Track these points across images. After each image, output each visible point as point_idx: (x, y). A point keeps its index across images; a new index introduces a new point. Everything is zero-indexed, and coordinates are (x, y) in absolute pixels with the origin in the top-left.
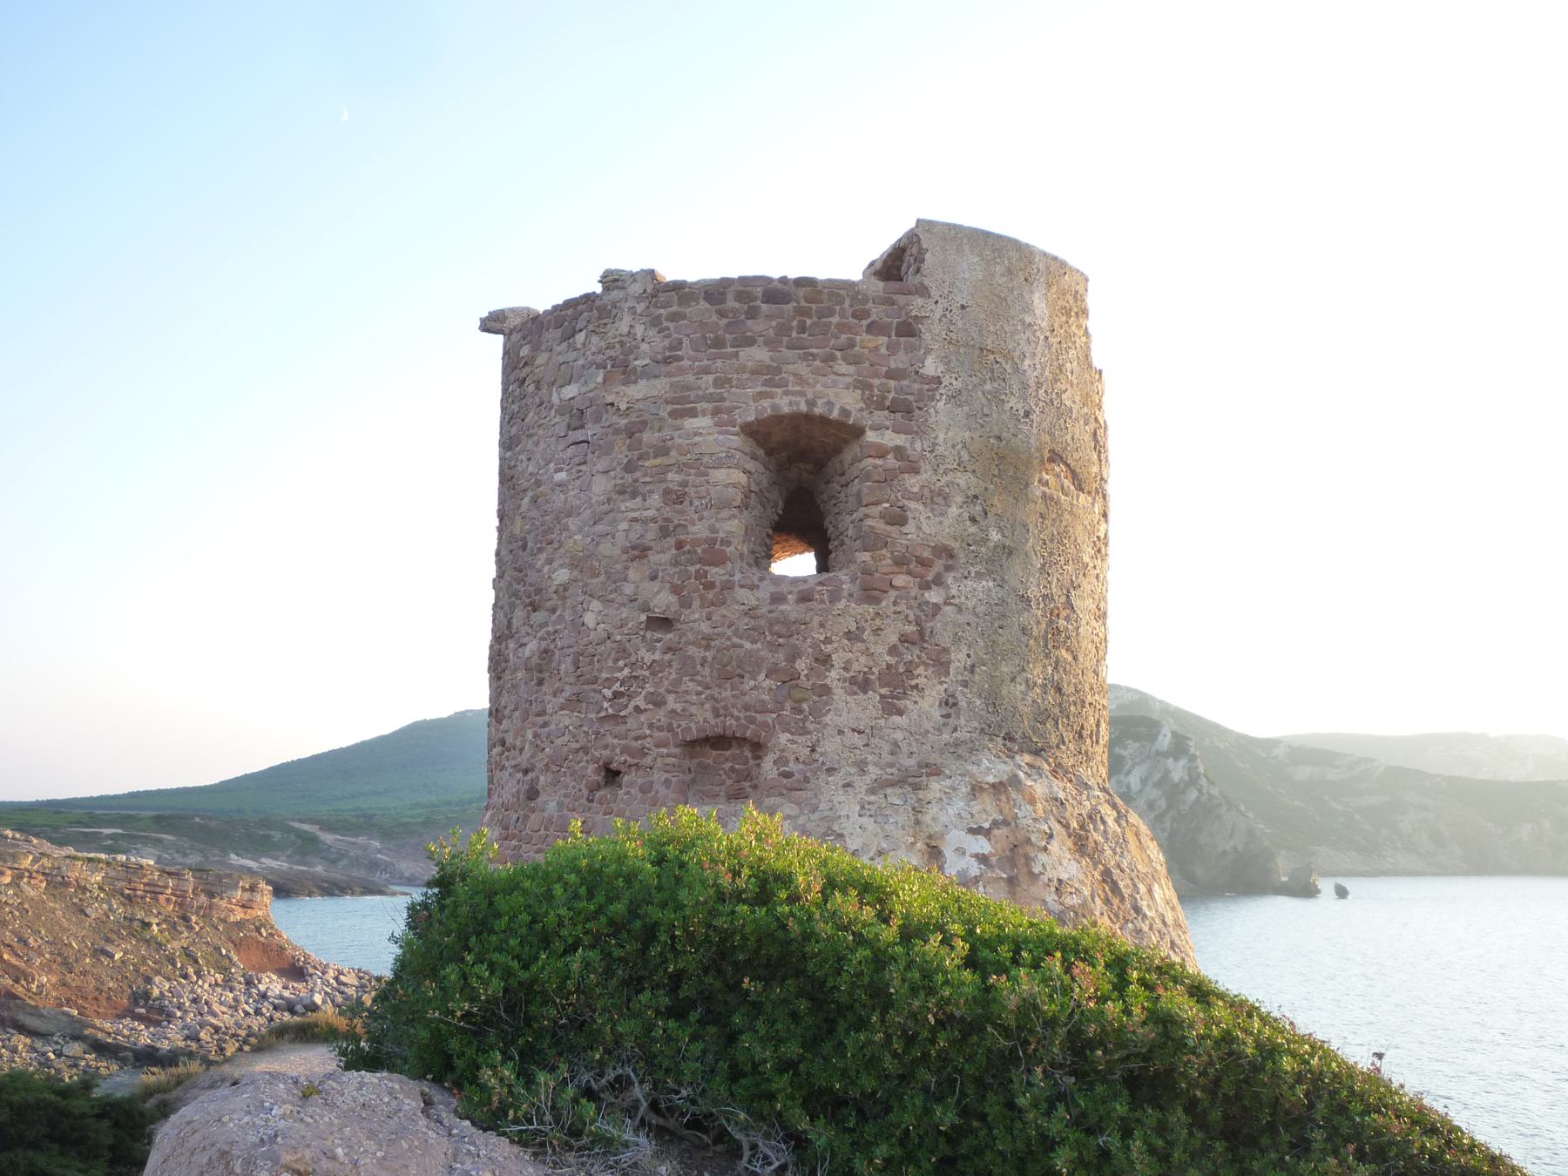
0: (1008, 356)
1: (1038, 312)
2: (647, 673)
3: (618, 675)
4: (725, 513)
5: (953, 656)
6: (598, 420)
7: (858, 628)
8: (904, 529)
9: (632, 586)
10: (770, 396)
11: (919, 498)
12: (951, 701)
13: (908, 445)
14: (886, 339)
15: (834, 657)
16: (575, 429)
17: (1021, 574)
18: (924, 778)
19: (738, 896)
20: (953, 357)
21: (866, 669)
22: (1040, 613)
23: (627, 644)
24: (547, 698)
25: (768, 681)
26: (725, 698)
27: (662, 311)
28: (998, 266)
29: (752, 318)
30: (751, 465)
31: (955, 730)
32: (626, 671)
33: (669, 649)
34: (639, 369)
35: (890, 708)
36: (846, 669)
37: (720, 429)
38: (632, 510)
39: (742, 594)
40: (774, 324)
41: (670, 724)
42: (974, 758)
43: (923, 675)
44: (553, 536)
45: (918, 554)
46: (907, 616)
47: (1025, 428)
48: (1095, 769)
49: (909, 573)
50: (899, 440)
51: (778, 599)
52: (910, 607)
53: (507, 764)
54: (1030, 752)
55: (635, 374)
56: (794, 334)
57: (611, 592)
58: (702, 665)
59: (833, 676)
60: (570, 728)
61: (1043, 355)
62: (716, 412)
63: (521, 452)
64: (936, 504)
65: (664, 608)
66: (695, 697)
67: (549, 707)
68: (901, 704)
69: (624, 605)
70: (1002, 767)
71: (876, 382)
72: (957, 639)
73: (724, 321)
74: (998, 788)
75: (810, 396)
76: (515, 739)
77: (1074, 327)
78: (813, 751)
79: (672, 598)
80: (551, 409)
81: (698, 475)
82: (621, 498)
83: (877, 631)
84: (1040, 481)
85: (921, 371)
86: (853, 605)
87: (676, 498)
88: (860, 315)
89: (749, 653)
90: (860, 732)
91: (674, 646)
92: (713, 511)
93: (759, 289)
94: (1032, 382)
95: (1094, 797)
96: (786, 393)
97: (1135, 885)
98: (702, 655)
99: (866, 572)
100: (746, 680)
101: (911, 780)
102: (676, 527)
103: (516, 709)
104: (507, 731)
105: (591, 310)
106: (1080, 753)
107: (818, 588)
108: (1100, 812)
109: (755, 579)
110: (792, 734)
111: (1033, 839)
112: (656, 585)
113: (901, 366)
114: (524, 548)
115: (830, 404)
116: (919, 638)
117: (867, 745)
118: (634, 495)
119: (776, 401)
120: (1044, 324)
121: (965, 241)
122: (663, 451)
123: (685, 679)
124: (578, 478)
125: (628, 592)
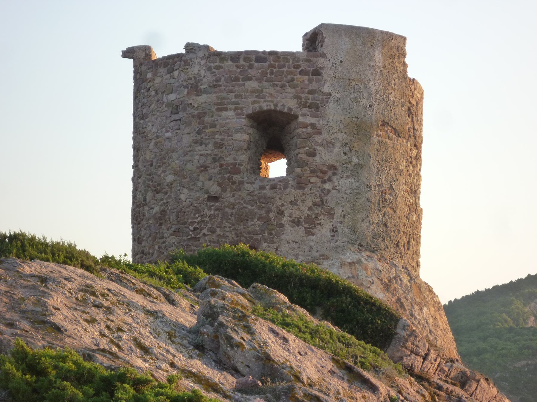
0: (362, 81)
1: (377, 60)
2: (208, 219)
3: (196, 220)
4: (240, 153)
5: (336, 211)
6: (185, 110)
7: (295, 200)
8: (315, 158)
10: (258, 102)
11: (321, 145)
12: (335, 229)
13: (317, 123)
14: (307, 77)
15: (285, 212)
16: (175, 114)
17: (367, 176)
18: (322, 260)
19: (238, 255)
20: (336, 84)
21: (299, 217)
22: (376, 192)
23: (199, 207)
24: (164, 231)
26: (240, 230)
27: (212, 64)
28: (358, 42)
29: (250, 69)
30: (251, 131)
31: (337, 241)
32: (199, 219)
33: (217, 209)
34: (203, 89)
35: (309, 232)
36: (290, 217)
37: (237, 117)
38: (200, 151)
39: (247, 186)
40: (260, 71)
41: (218, 241)
42: (343, 253)
43: (323, 219)
44: (165, 161)
45: (321, 169)
46: (316, 195)
47: (370, 112)
48: (406, 261)
49: (317, 176)
51: (262, 188)
52: (317, 191)
53: (145, 261)
54: (370, 251)
55: (201, 92)
56: (268, 76)
57: (192, 185)
59: (285, 220)
60: (175, 243)
61: (379, 79)
62: (236, 109)
63: (149, 122)
64: (329, 147)
66: (228, 229)
67: (165, 235)
68: (312, 231)
69: (198, 191)
70: (355, 256)
72: (337, 204)
73: (239, 70)
74: (351, 264)
75: (275, 102)
76: (150, 249)
77: (396, 64)
78: (277, 250)
79: (218, 188)
80: (163, 104)
81: (228, 136)
82: (196, 145)
83: (303, 201)
84: (377, 135)
85: (322, 91)
86: (293, 190)
87: (219, 146)
88: (297, 67)
90: (296, 242)
93: (253, 56)
94: (373, 92)
95: (399, 270)
96: (265, 101)
97: (412, 306)
99: (299, 176)
100: (249, 221)
101: (316, 261)
102: (220, 158)
103: (149, 237)
104: (145, 247)
105: (181, 61)
106: (397, 253)
107: (279, 183)
108: (400, 276)
109: (253, 179)
110: (268, 243)
111: (364, 284)
112: (211, 183)
113: (314, 88)
114: (152, 165)
115: (284, 106)
116: (321, 204)
117: (299, 248)
118: (201, 144)
119: (261, 104)
120: (380, 65)
121: (343, 32)
122: (213, 126)
124: (176, 136)
125: (199, 186)
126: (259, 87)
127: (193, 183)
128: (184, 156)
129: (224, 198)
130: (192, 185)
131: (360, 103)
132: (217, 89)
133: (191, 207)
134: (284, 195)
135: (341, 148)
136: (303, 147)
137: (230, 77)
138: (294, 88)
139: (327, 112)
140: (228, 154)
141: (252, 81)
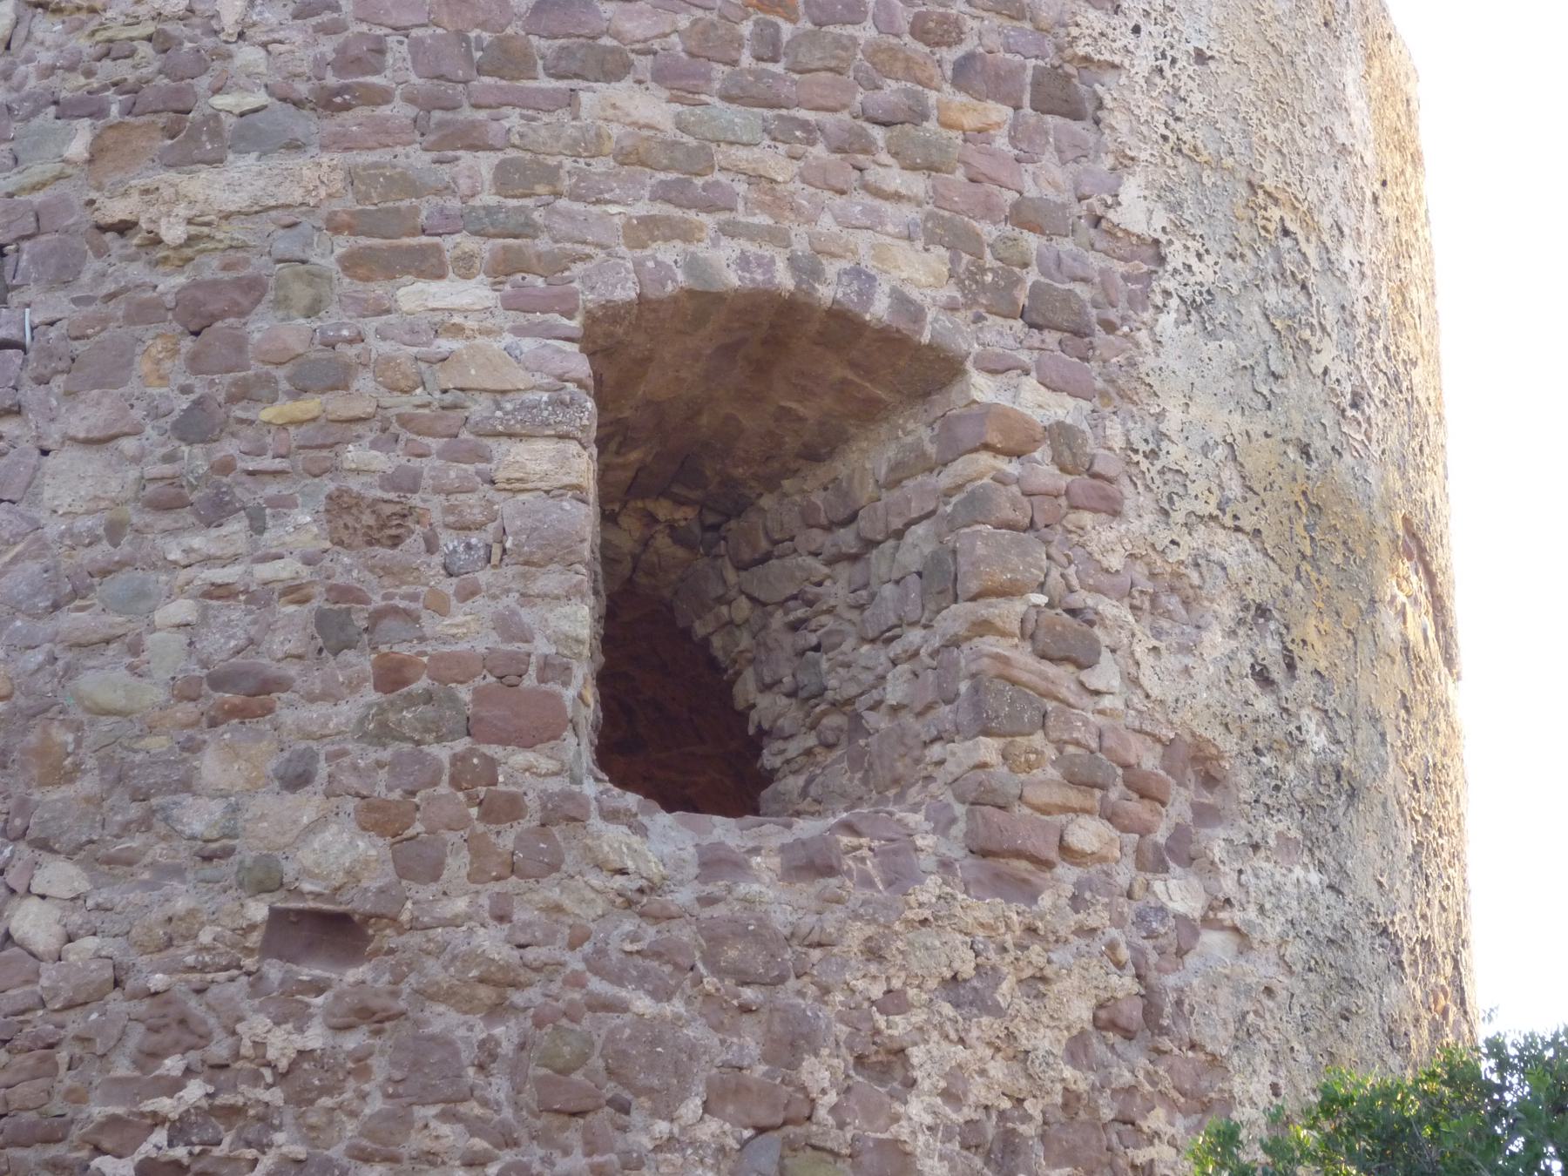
2: (276, 1096)
9: (217, 808)
10: (687, 234)
14: (1007, 112)
15: (917, 1054)
21: (1006, 1104)
23: (193, 1003)
25: (713, 1126)
32: (195, 1091)
33: (367, 1015)
34: (229, 122)
37: (522, 319)
38: (208, 561)
46: (1112, 946)
49: (1111, 816)
50: (1064, 409)
52: (1118, 922)
55: (216, 134)
57: (126, 828)
58: (481, 1067)
65: (339, 878)
69: (177, 872)
71: (988, 230)
75: (801, 246)
79: (370, 847)
82: (166, 521)
85: (1111, 215)
89: (653, 1033)
91: (376, 1003)
92: (510, 571)
96: (730, 230)
98: (480, 1033)
100: (636, 1118)
102: (378, 616)
112: (307, 805)
118: (216, 511)
119: (701, 250)
123: (421, 1112)
126: (682, 126)
127: (135, 811)
128: (56, 606)
129: (415, 926)
130: (126, 828)
131: (1314, 357)
132: (351, 121)
133: (117, 1003)
134: (898, 926)
135: (1241, 631)
136: (1007, 592)
137: (461, 36)
138: (931, 168)
139: (1148, 363)
140: (449, 586)
141: (628, 82)
